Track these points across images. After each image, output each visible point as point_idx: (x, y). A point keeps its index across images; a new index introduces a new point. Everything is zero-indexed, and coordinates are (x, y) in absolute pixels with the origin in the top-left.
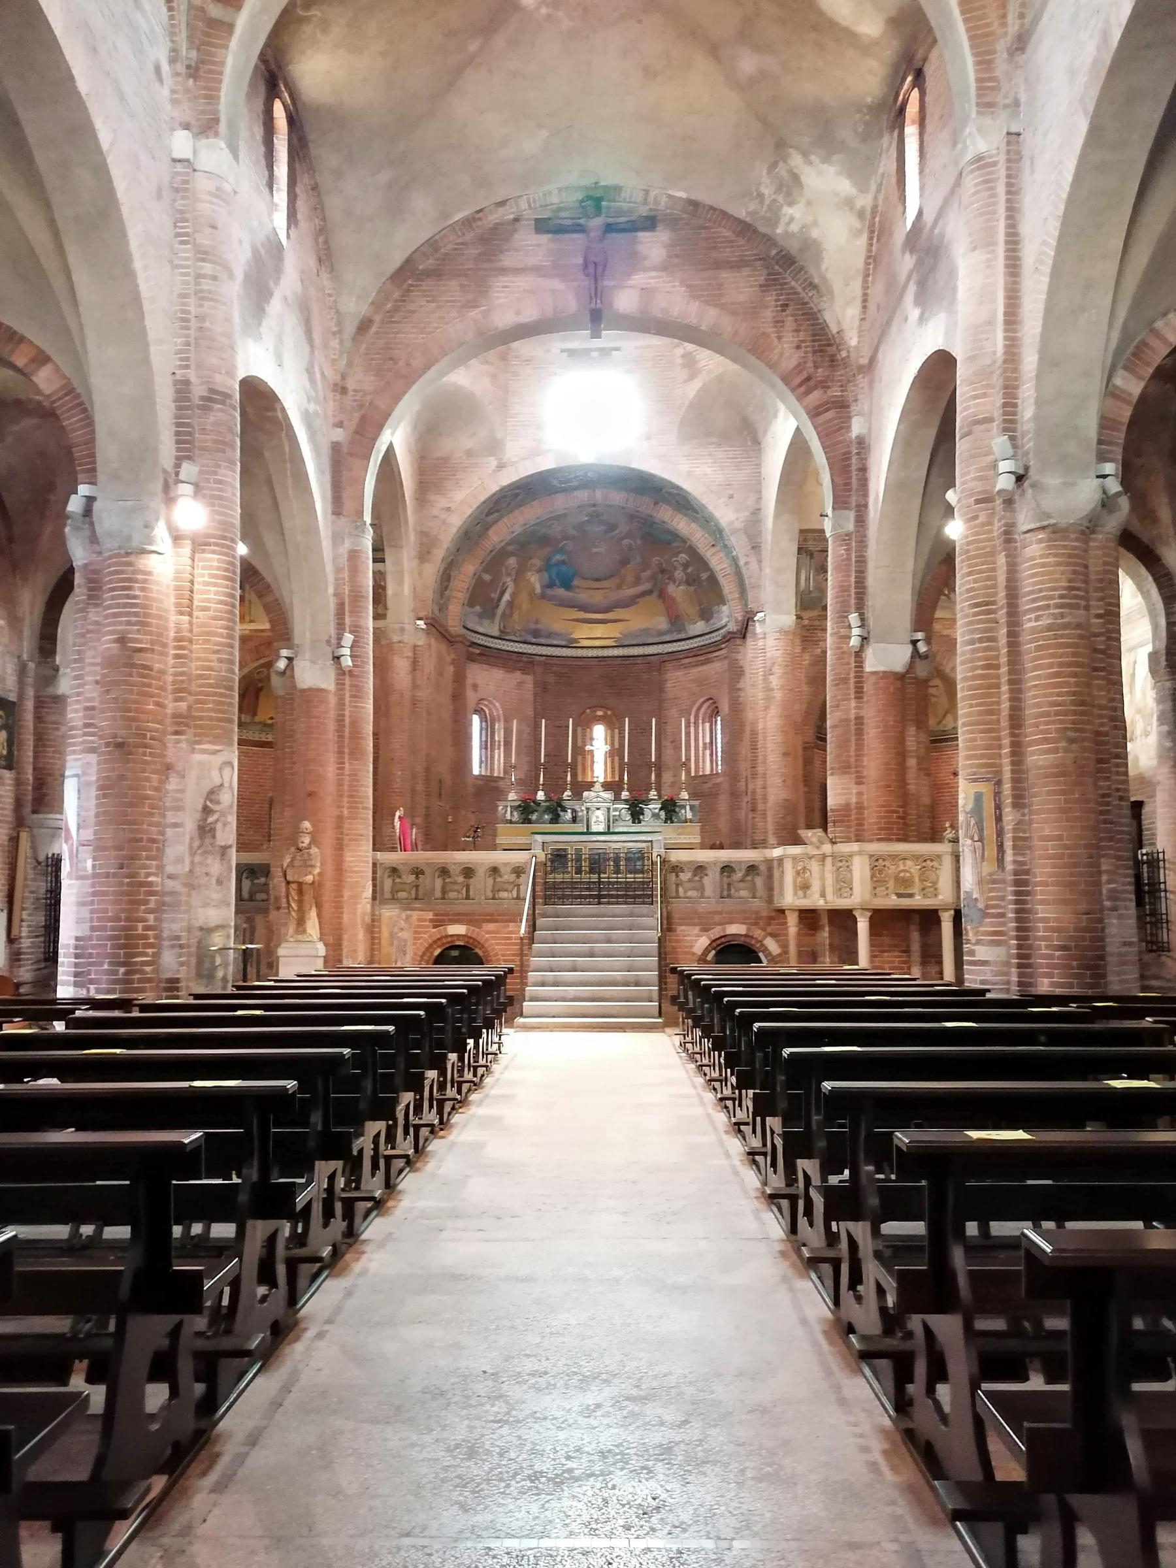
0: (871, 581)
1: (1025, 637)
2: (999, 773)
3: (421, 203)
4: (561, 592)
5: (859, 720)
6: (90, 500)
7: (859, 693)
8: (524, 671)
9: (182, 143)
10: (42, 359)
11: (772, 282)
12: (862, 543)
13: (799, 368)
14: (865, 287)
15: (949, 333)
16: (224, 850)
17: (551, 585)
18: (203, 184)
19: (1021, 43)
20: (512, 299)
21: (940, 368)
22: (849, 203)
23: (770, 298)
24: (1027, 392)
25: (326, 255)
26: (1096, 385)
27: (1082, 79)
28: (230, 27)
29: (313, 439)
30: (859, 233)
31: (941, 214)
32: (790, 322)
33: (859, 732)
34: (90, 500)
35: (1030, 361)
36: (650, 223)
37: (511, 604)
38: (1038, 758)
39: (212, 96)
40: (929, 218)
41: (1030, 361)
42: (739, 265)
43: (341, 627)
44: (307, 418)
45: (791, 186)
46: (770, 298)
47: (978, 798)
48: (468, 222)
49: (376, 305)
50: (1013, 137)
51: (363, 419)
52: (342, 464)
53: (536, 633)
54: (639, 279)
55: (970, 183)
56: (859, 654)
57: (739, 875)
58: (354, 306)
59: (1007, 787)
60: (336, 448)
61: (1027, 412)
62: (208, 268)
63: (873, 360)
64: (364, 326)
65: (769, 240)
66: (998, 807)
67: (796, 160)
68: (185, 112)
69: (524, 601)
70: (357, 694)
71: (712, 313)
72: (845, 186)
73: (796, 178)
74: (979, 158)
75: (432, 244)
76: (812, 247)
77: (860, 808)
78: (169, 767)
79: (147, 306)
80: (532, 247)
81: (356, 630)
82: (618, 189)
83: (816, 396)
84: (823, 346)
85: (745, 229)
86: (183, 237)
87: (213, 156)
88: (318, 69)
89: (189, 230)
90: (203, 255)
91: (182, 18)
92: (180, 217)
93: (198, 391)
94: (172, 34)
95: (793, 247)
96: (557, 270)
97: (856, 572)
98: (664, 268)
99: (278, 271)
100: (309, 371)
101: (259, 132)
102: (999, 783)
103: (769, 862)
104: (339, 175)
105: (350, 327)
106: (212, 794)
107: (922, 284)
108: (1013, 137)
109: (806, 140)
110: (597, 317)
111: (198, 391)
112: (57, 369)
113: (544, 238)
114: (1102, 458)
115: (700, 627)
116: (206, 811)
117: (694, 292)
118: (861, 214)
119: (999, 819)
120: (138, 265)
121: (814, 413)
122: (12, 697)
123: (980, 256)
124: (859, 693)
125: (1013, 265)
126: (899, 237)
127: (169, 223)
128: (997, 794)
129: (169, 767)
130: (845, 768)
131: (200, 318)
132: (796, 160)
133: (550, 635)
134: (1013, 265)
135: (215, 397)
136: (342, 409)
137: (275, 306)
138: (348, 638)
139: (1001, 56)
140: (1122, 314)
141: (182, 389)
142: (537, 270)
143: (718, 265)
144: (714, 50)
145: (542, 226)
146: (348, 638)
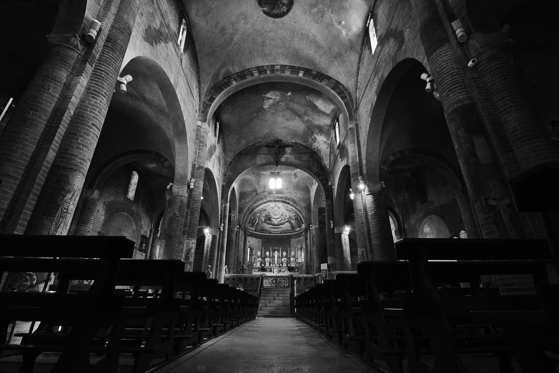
0: (335, 214)
1: (369, 216)
2: (366, 246)
3: (243, 142)
4: (268, 221)
5: (334, 244)
6: (172, 186)
7: (334, 238)
8: (260, 238)
9: (199, 123)
10: (166, 160)
11: (311, 157)
12: (332, 206)
13: (318, 172)
14: (330, 157)
15: (348, 161)
16: (191, 263)
17: (266, 220)
18: (202, 130)
19: (357, 109)
20: (260, 159)
21: (347, 167)
22: (326, 142)
23: (311, 160)
24: (364, 168)
25: (224, 150)
26: (378, 166)
27: (369, 112)
28: (211, 105)
29: (218, 183)
30: (328, 148)
31: (344, 141)
32: (315, 164)
33: (334, 247)
34: (172, 186)
35: (364, 162)
36: (288, 146)
37: (257, 224)
38: (374, 242)
39: (206, 116)
40: (341, 142)
41: (364, 162)
42: (304, 154)
43: (221, 223)
44: (218, 178)
45: (315, 140)
46: (311, 160)
47: (362, 251)
48: (252, 145)
49: (233, 160)
50: (357, 125)
51: (229, 181)
52: (225, 189)
53: (263, 230)
54: (286, 156)
55: (349, 132)
56: (333, 229)
57: (308, 281)
58: (229, 160)
59: (368, 249)
60: (223, 186)
61: (365, 172)
62: (201, 144)
63: (332, 170)
64: (231, 163)
65: (311, 149)
66: (367, 254)
67: (315, 135)
68: (201, 118)
69: (260, 222)
70: (223, 237)
71: (300, 162)
72: (325, 140)
73: (315, 138)
74: (351, 128)
75: (245, 149)
76: (319, 151)
77: (335, 264)
78: (181, 243)
79: (189, 149)
80: (265, 150)
81: (224, 223)
82: (281, 140)
83: (321, 177)
84: (322, 167)
85: (306, 147)
86: (197, 139)
87: (205, 126)
88: (225, 117)
89: (200, 140)
90: (201, 142)
91: (202, 103)
92: (197, 135)
93: (197, 166)
94: (200, 105)
95: (316, 150)
96: (269, 154)
97: (333, 89)
98: (290, 154)
99: (215, 150)
100: (219, 170)
101: (214, 126)
102: (367, 249)
103: (315, 277)
104: (228, 136)
105: (228, 163)
106: (190, 250)
107: (341, 154)
108: (357, 125)
109: (317, 131)
110: (277, 163)
111: (197, 166)
112: (169, 162)
113: (267, 148)
114: (381, 181)
115: (298, 229)
116: (188, 253)
117: (296, 158)
118: (328, 145)
119: (367, 257)
120: (188, 141)
121: (321, 181)
122: (148, 237)
123: (352, 144)
124: (334, 238)
125: (359, 146)
126: (336, 147)
127: (195, 136)
128: (366, 251)
129: (181, 243)
130: (331, 255)
131: (199, 153)
132: (315, 135)
133: (266, 231)
134: (359, 146)
135: (200, 167)
136: (225, 178)
137: (214, 156)
138: (222, 225)
139: (353, 112)
140: (381, 154)
141: (194, 166)
142: (266, 154)
143: (301, 153)
144: (300, 116)
145: (266, 146)
146: (222, 225)
